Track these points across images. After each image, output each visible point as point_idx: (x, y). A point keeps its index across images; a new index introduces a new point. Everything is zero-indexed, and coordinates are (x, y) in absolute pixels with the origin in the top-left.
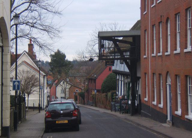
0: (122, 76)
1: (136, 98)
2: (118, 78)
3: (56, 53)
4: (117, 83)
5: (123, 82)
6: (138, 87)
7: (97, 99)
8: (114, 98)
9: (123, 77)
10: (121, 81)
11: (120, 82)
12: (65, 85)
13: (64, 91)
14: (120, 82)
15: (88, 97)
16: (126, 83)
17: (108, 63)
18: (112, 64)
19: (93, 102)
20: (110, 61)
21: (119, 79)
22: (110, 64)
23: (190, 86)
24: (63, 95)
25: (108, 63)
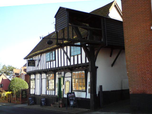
25: (30, 64)
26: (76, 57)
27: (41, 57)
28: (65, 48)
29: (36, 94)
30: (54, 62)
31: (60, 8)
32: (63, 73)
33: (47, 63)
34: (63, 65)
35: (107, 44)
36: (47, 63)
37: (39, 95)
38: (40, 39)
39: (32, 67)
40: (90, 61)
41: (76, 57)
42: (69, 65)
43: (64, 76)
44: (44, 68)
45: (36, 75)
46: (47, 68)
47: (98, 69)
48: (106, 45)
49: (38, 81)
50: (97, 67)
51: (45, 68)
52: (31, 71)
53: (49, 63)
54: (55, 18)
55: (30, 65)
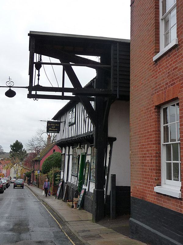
0: (71, 147)
1: (85, 181)
2: (63, 152)
3: (14, 144)
4: (63, 160)
5: (71, 157)
6: (110, 158)
7: (39, 179)
8: (57, 180)
9: (72, 148)
10: (69, 155)
11: (67, 157)
12: (17, 167)
13: (16, 172)
14: (67, 157)
15: (34, 178)
16: (78, 155)
17: (50, 129)
18: (57, 129)
19: (37, 183)
20: (53, 126)
21: (65, 154)
22: (54, 129)
23: (169, 165)
24: (15, 176)
25: (50, 129)
50: (115, 139)
55: (51, 130)
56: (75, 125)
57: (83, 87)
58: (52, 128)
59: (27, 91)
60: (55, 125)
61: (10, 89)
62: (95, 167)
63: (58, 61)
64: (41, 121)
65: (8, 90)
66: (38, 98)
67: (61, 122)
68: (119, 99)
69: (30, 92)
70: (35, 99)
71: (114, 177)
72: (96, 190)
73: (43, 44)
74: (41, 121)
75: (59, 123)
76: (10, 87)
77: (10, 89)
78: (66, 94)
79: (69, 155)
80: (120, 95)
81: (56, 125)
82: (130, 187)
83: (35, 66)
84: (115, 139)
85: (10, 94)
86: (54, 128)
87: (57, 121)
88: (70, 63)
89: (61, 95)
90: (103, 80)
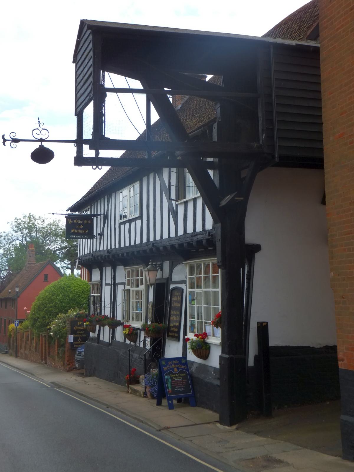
10: (115, 285)
11: (107, 291)
14: (107, 291)
17: (73, 230)
18: (87, 231)
20: (79, 224)
25: (73, 230)
26: (190, 206)
27: (108, 205)
28: (165, 172)
29: (101, 339)
30: (139, 222)
31: (83, 23)
32: (167, 265)
33: (122, 227)
34: (127, 244)
35: (277, 156)
36: (122, 227)
37: (109, 344)
38: (4, 144)
39: (89, 240)
40: (219, 225)
41: (190, 206)
42: (123, 247)
43: (168, 278)
44: (134, 237)
45: (104, 268)
46: (122, 245)
47: (258, 257)
48: (273, 157)
49: (108, 288)
50: (257, 248)
51: (117, 246)
52: (133, 243)
53: (127, 225)
54: (75, 64)
55: (74, 234)
56: (139, 222)
57: (83, 145)
58: (78, 229)
59: (72, 149)
60: (83, 222)
61: (41, 147)
62: (102, 308)
63: (137, 84)
64: (53, 214)
65: (38, 147)
66: (102, 166)
67: (96, 216)
68: (278, 165)
69: (80, 151)
70: (94, 167)
71: (263, 329)
72: (227, 356)
73: (108, 48)
74: (53, 214)
75: (90, 218)
76: (41, 140)
77: (41, 147)
78: (104, 154)
79: (115, 285)
80: (280, 157)
81: (85, 222)
82: (334, 349)
83: (91, 92)
84: (257, 248)
85: (42, 156)
86: (81, 229)
87: (77, 213)
88: (165, 89)
89: (94, 156)
90: (238, 121)
